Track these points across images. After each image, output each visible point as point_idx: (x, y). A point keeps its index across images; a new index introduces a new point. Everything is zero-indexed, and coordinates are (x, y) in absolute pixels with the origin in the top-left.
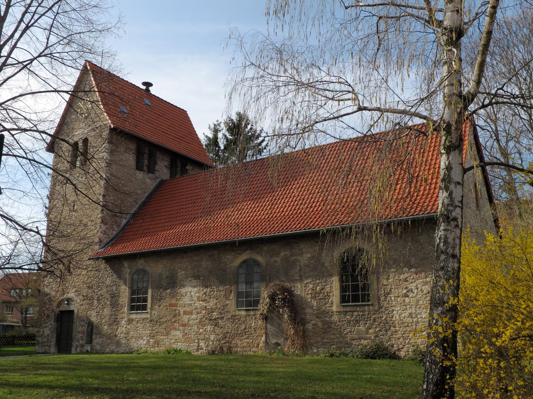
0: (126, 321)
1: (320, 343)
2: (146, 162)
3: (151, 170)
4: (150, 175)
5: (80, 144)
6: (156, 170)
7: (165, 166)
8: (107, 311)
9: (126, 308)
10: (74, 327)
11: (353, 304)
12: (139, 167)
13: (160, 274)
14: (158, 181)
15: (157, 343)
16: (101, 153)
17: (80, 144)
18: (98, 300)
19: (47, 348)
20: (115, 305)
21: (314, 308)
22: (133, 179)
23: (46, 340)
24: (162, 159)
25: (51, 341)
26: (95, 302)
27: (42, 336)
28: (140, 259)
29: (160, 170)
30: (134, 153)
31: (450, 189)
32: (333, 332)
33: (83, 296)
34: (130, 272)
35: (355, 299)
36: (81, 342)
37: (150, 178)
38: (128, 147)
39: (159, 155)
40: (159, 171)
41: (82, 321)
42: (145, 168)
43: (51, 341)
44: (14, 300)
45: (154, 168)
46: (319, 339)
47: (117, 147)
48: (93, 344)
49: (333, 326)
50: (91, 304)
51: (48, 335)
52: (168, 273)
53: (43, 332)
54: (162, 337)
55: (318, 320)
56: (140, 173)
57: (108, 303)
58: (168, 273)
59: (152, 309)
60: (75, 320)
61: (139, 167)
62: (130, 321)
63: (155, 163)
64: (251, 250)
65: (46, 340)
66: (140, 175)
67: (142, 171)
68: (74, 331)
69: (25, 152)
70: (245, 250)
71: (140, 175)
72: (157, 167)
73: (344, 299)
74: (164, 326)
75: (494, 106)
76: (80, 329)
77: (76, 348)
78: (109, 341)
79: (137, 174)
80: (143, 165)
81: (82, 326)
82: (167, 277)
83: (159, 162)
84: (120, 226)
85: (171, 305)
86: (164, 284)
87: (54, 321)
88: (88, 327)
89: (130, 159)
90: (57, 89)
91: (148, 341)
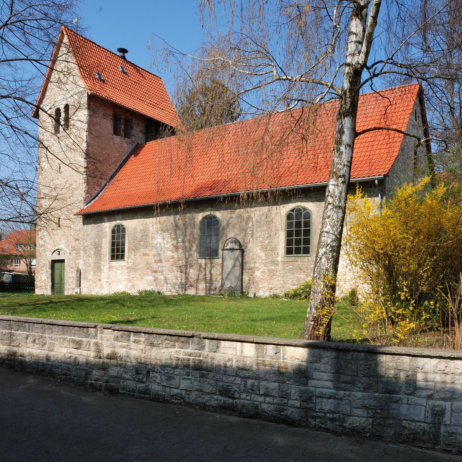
0: (107, 268)
1: (267, 288)
2: (123, 127)
3: (127, 135)
4: (127, 139)
5: (62, 110)
6: (133, 135)
7: (141, 131)
8: (91, 260)
9: (107, 257)
10: (66, 273)
11: (296, 255)
12: (116, 132)
13: (135, 228)
14: (134, 145)
15: (133, 286)
16: (81, 117)
17: (62, 110)
18: (84, 250)
19: (45, 291)
20: (98, 254)
21: (263, 258)
22: (111, 143)
23: (43, 284)
24: (138, 125)
25: (47, 285)
26: (82, 252)
27: (40, 281)
28: (117, 215)
29: (136, 135)
30: (111, 119)
31: (341, 150)
32: (277, 279)
33: (72, 247)
34: (110, 226)
35: (298, 251)
36: (72, 285)
37: (126, 142)
38: (106, 113)
39: (134, 121)
40: (135, 136)
41: (71, 268)
42: (122, 133)
43: (47, 285)
44: (20, 254)
45: (130, 133)
46: (266, 284)
47: (95, 113)
48: (81, 287)
49: (278, 274)
50: (78, 254)
51: (45, 280)
52: (141, 227)
53: (41, 277)
54: (137, 281)
55: (265, 268)
56: (117, 138)
57: (93, 253)
58: (141, 227)
59: (128, 258)
60: (66, 268)
61: (116, 132)
62: (110, 268)
63: (132, 128)
64: (212, 207)
65: (43, 284)
66: (117, 139)
67: (119, 135)
68: (65, 276)
69: (6, 117)
70: (207, 207)
71: (118, 140)
72: (133, 132)
73: (289, 252)
74: (139, 272)
75: (65, 78)
76: (70, 275)
77: (68, 291)
78: (95, 285)
79: (115, 139)
80: (120, 130)
81: (72, 272)
82: (141, 231)
83: (135, 128)
84: (101, 186)
85: (145, 255)
86: (138, 236)
87: (49, 269)
88: (77, 273)
89: (108, 125)
90: (29, 57)
91: (126, 285)
